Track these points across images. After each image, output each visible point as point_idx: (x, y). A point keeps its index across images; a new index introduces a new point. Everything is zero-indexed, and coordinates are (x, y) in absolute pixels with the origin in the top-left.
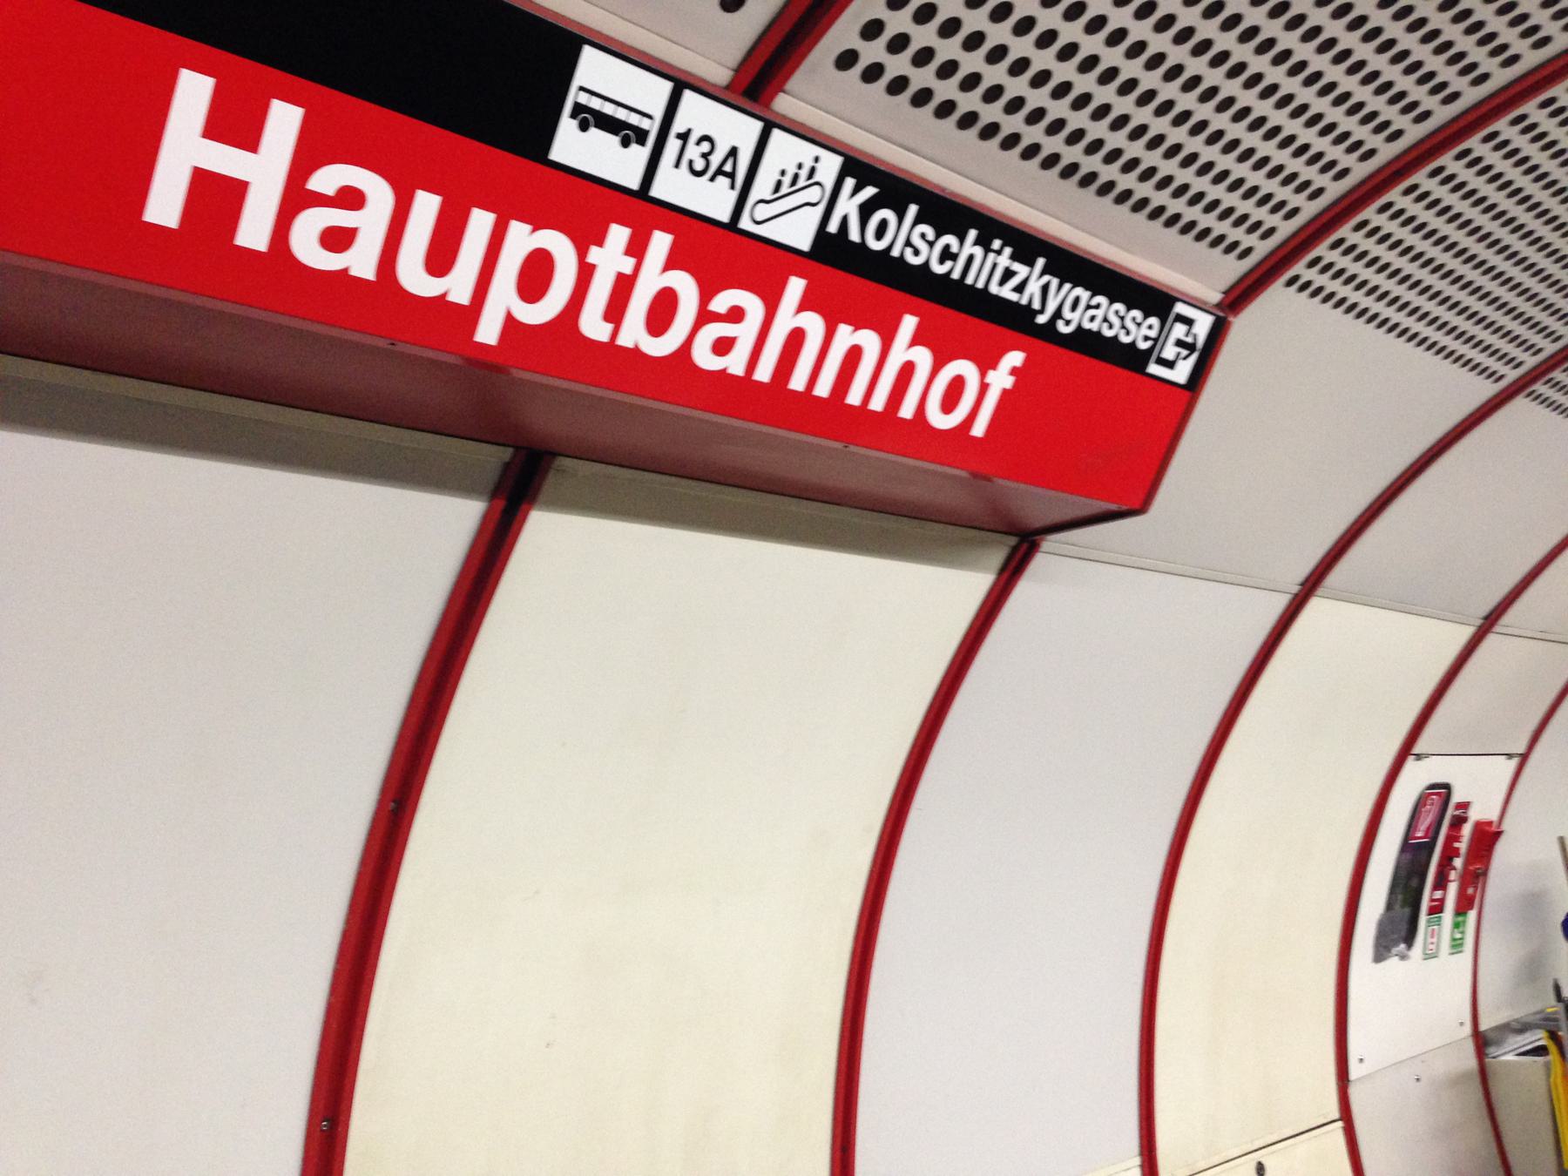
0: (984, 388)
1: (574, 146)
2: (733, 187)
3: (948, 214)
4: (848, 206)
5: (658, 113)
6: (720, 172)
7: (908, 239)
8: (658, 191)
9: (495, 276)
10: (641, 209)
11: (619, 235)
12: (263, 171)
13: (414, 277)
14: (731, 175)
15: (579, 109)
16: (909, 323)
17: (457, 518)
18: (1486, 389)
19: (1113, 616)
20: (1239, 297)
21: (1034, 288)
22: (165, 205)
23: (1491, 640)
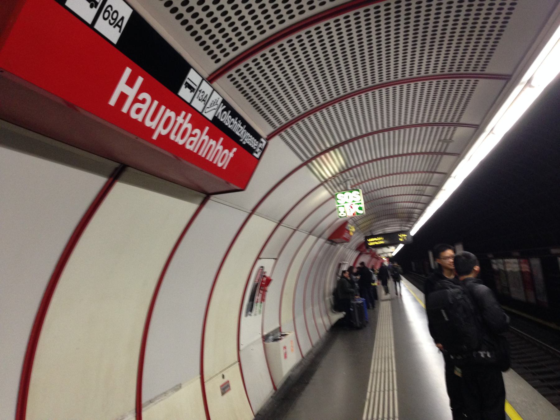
0: (176, 121)
1: (184, 93)
2: (120, 32)
3: (235, 114)
5: (198, 84)
6: (117, 25)
7: (227, 119)
8: (96, 27)
10: (188, 107)
12: (131, 93)
14: (120, 27)
15: (187, 83)
17: (100, 181)
19: (222, 212)
20: (270, 137)
21: (242, 133)
22: (112, 102)
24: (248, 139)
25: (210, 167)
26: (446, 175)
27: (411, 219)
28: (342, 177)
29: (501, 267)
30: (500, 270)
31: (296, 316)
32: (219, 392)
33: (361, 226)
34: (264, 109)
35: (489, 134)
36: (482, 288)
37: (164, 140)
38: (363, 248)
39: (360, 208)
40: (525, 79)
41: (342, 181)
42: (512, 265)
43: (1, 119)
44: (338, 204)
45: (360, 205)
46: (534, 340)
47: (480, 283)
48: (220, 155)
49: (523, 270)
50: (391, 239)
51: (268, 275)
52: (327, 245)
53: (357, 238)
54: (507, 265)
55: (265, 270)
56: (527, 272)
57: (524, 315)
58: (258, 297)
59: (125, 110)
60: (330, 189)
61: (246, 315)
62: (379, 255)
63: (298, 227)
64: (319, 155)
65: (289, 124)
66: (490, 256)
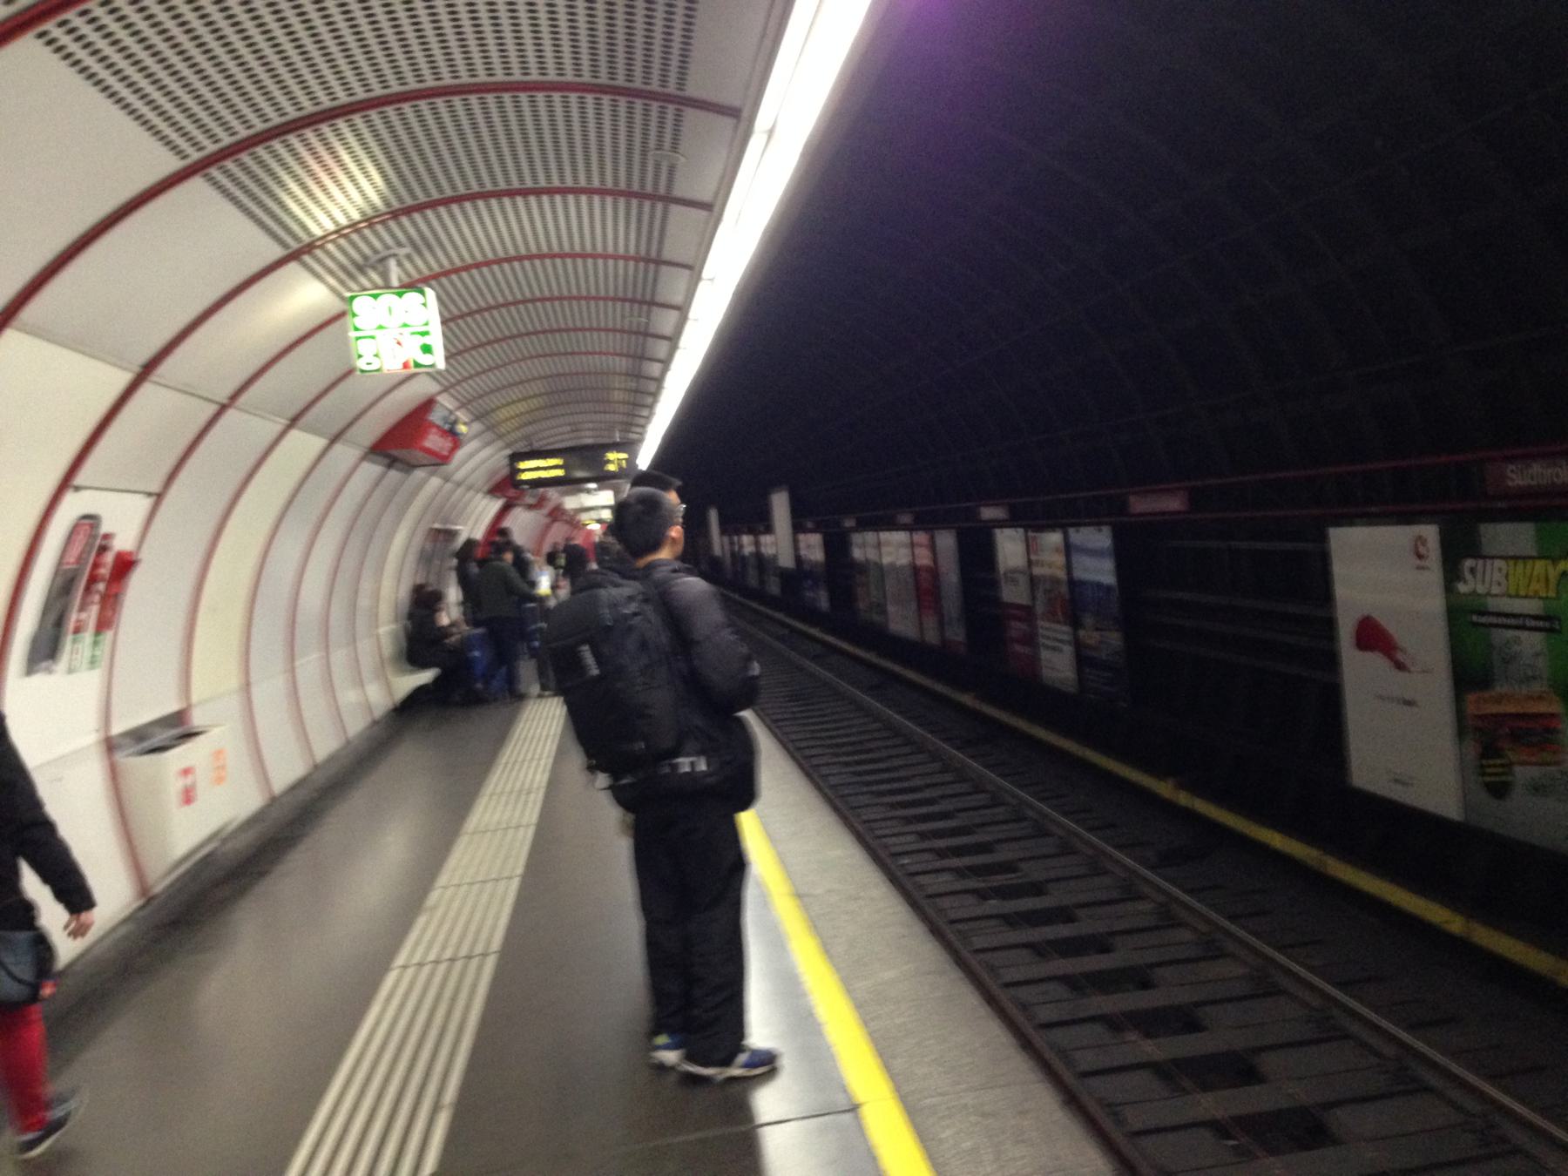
18: (173, 164)
23: (147, 389)
29: (871, 554)
31: (254, 677)
36: (694, 585)
39: (427, 349)
41: (362, 259)
44: (356, 329)
45: (426, 340)
47: (690, 572)
49: (919, 562)
50: (585, 462)
54: (884, 550)
55: (105, 528)
57: (911, 674)
63: (234, 397)
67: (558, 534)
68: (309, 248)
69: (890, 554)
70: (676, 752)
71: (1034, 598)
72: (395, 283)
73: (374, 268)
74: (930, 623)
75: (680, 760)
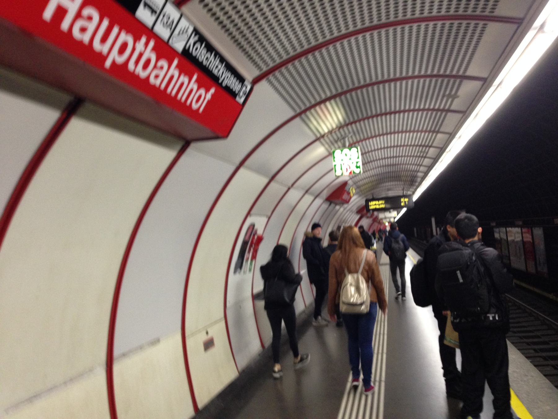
3: (210, 48)
4: (192, 41)
7: (201, 53)
8: (520, 229)
9: (115, 47)
10: (150, 33)
11: (144, 40)
13: (97, 46)
16: (195, 77)
17: (52, 116)
19: (204, 162)
20: (256, 81)
22: (48, 14)
24: (229, 80)
25: (185, 108)
26: (451, 136)
27: (413, 181)
28: (340, 133)
30: (501, 239)
32: (202, 348)
33: (362, 188)
34: (247, 47)
35: (496, 89)
37: (121, 70)
38: (364, 211)
39: (357, 167)
40: (537, 23)
41: (338, 139)
42: (514, 234)
43: (10, 66)
46: (538, 314)
48: (196, 95)
49: (525, 240)
50: (393, 203)
51: (260, 232)
52: (325, 206)
53: (356, 201)
56: (530, 242)
58: (248, 255)
59: (65, 25)
60: (327, 146)
61: (235, 272)
62: (382, 219)
63: (293, 185)
64: (314, 106)
65: (277, 67)
66: (494, 224)
67: (376, 227)
68: (323, 136)
69: (511, 236)
70: (489, 312)
71: (369, 230)
72: (347, 144)
73: (340, 141)
74: (531, 264)
75: (488, 315)
